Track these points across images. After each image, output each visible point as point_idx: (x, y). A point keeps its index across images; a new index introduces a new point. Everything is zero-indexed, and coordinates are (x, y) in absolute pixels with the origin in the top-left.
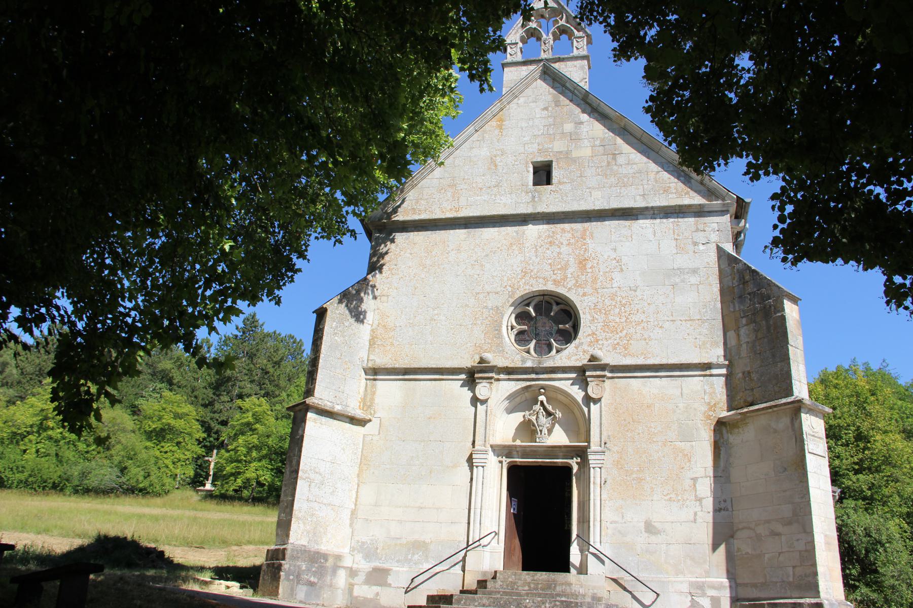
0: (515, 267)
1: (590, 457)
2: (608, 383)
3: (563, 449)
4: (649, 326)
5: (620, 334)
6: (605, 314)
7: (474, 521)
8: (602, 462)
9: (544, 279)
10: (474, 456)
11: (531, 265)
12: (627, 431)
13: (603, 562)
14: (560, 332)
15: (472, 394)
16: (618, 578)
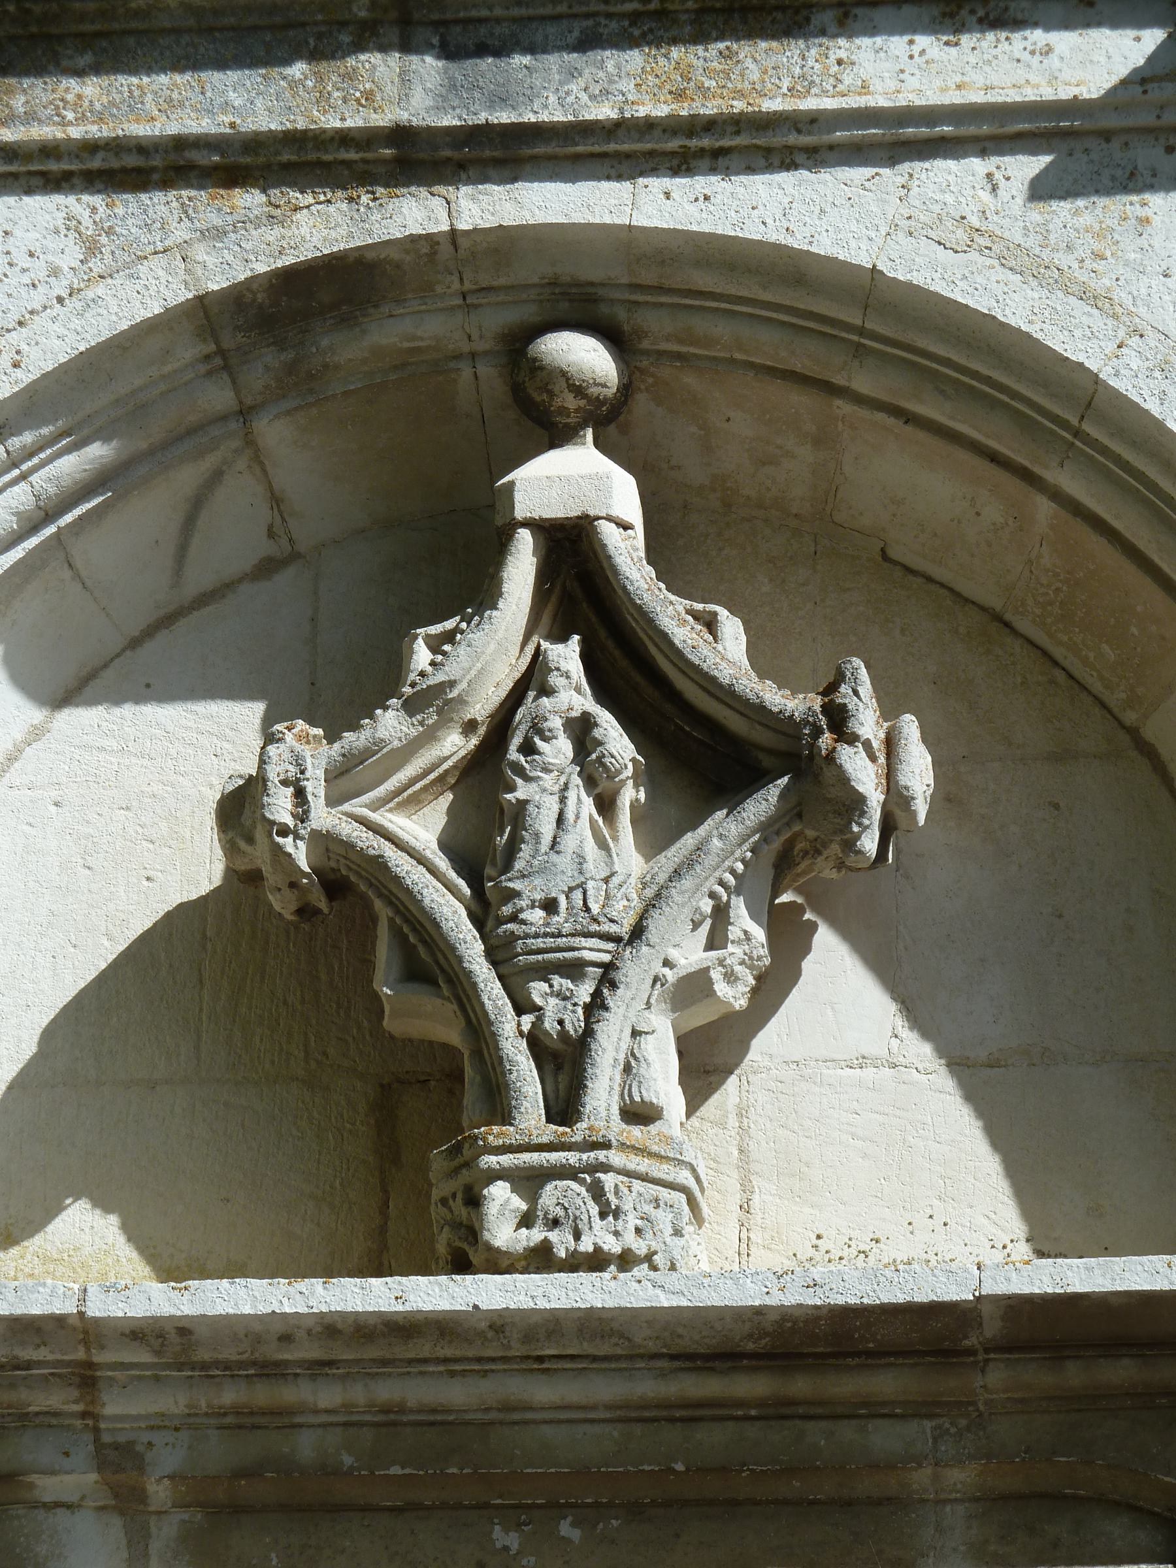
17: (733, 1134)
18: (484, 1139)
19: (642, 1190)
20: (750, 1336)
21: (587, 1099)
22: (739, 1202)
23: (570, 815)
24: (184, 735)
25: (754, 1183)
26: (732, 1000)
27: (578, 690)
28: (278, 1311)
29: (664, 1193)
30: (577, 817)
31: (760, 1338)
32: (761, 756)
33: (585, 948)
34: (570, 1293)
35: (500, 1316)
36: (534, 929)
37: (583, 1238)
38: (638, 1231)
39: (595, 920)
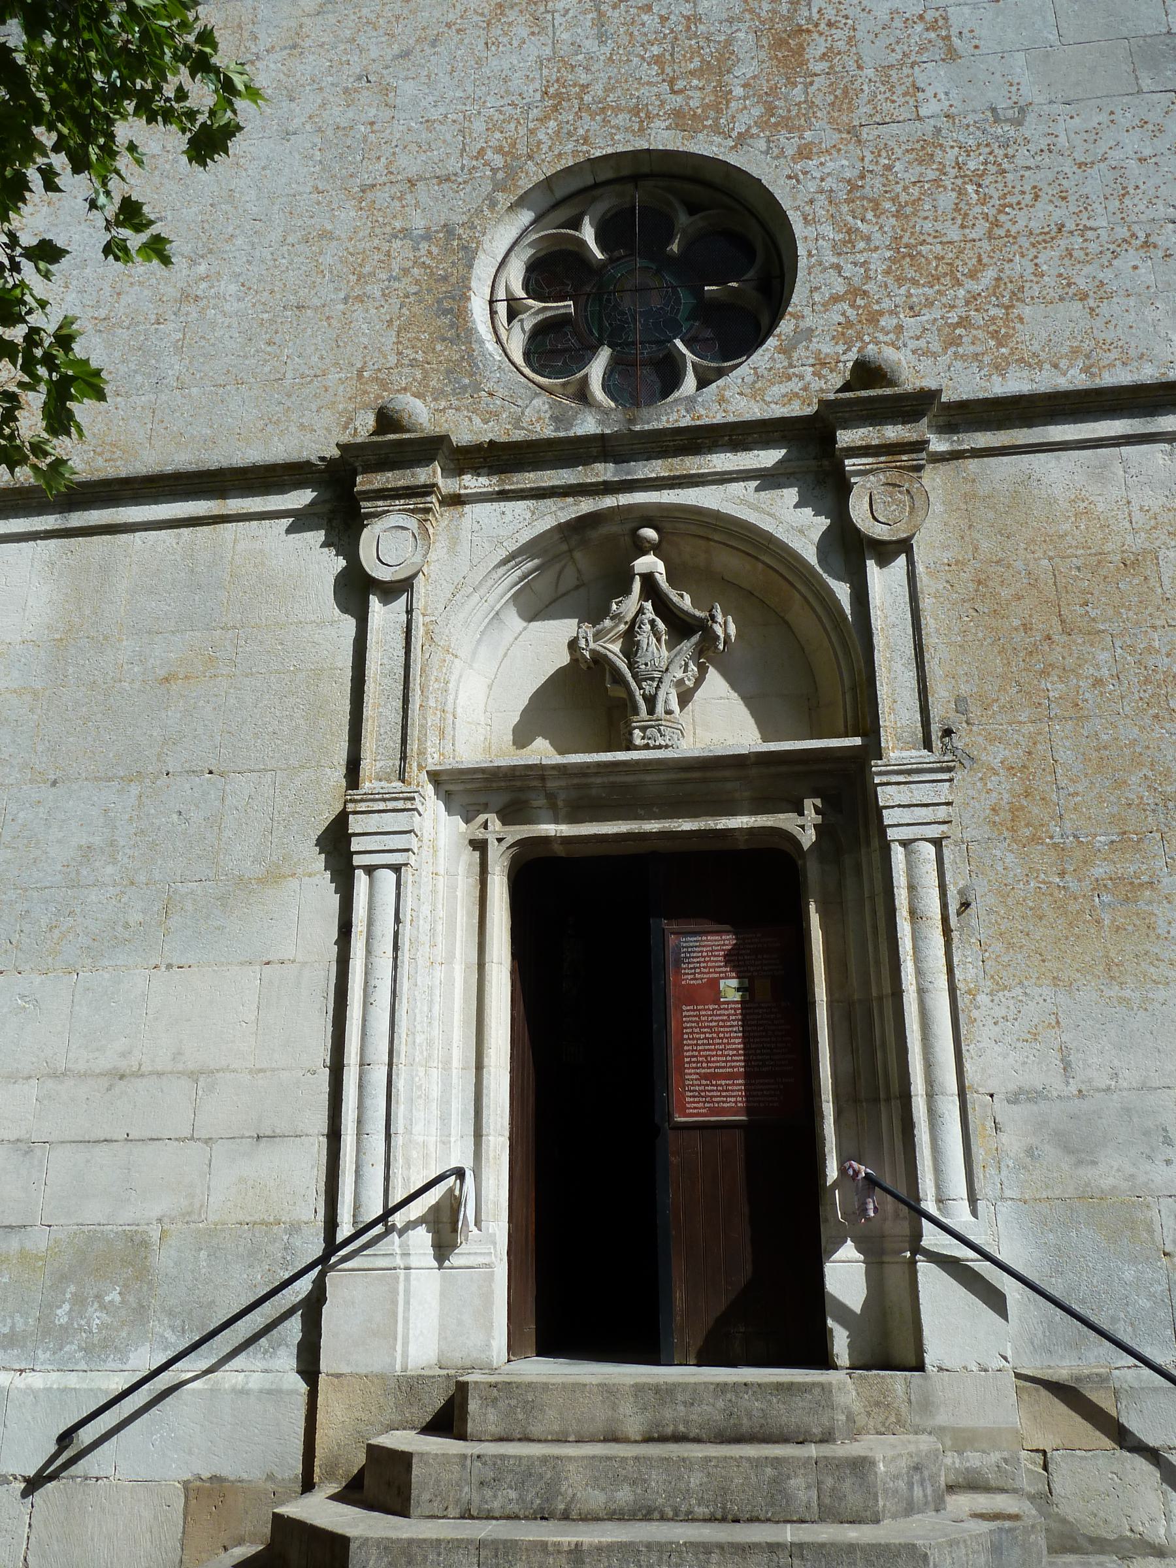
0: (516, 82)
1: (885, 796)
2: (934, 479)
3: (754, 771)
4: (1093, 247)
5: (971, 285)
6: (897, 215)
7: (360, 1122)
8: (942, 813)
9: (635, 111)
10: (356, 824)
11: (579, 70)
12: (1044, 673)
13: (996, 1301)
14: (707, 311)
15: (341, 563)
16: (1078, 1379)
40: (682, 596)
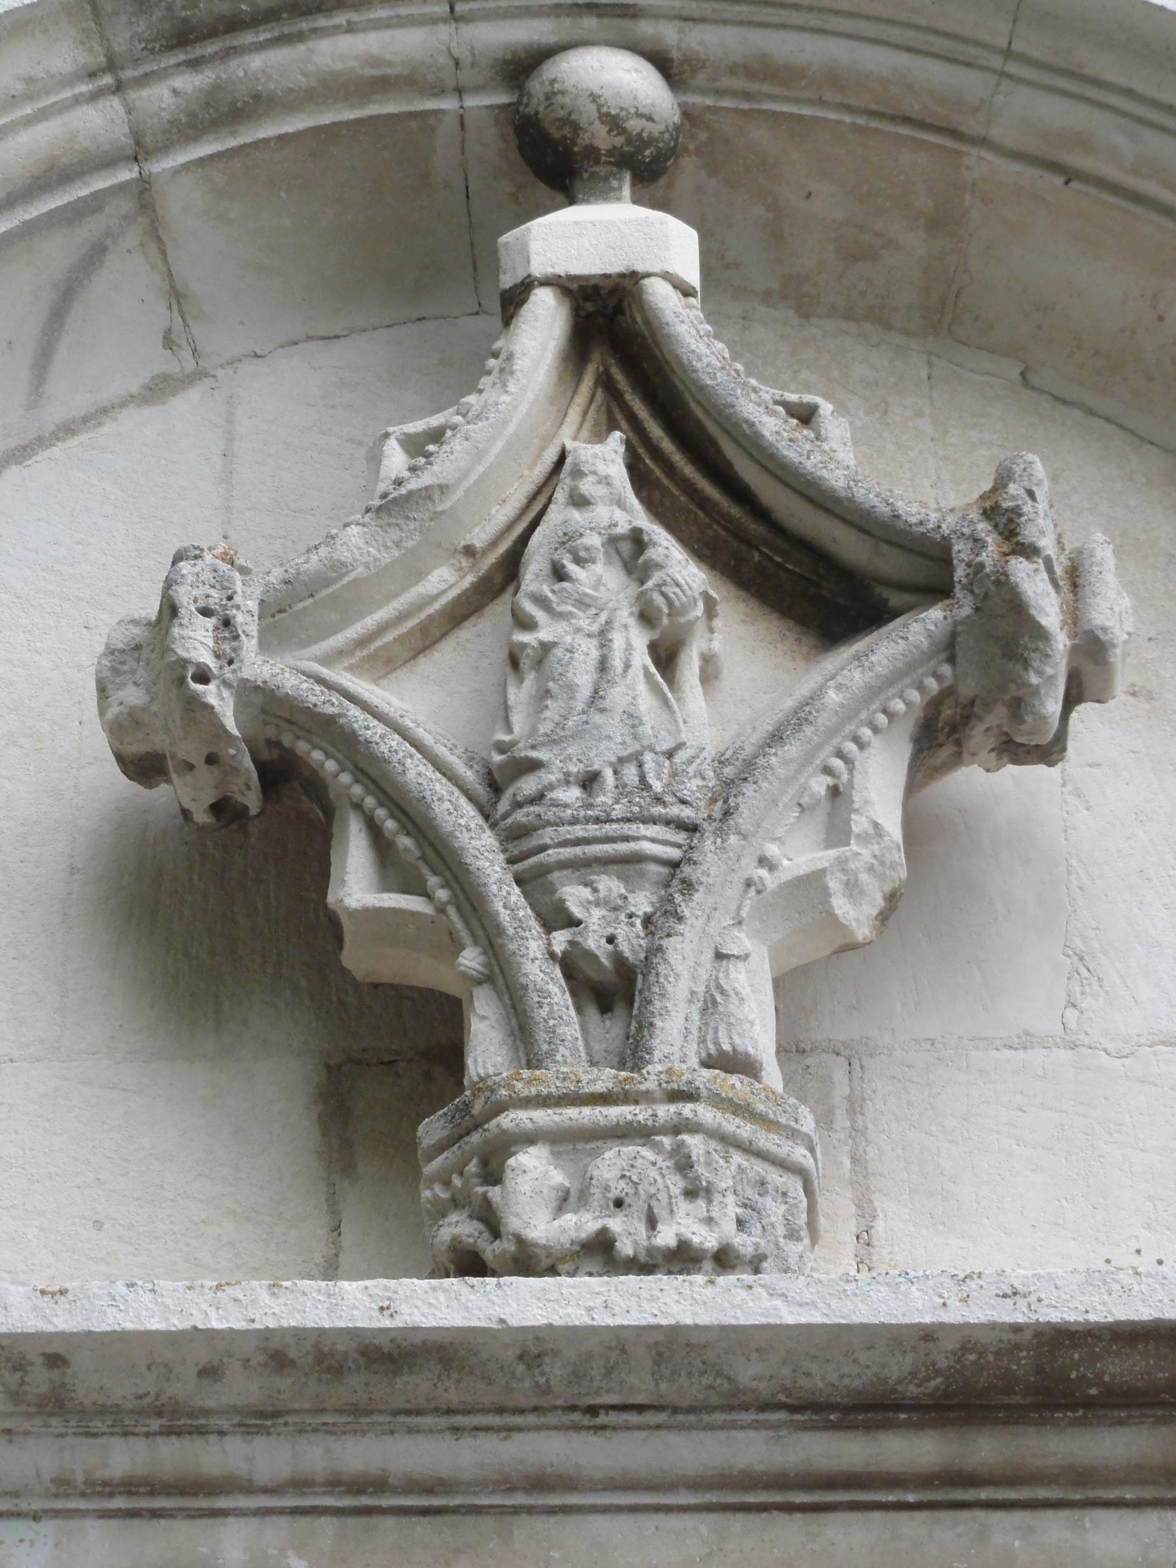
17: (842, 1136)
18: (509, 1086)
19: (745, 1164)
20: (913, 1374)
21: (655, 1042)
22: (855, 1231)
23: (617, 663)
24: (43, 601)
25: (876, 1204)
26: (854, 924)
27: (620, 504)
28: (201, 1326)
29: (775, 1177)
30: (627, 666)
31: (928, 1379)
32: (885, 593)
33: (645, 838)
34: (644, 1304)
35: (537, 1338)
36: (569, 812)
37: (660, 1227)
38: (740, 1223)
39: (658, 800)
40: (805, 416)
